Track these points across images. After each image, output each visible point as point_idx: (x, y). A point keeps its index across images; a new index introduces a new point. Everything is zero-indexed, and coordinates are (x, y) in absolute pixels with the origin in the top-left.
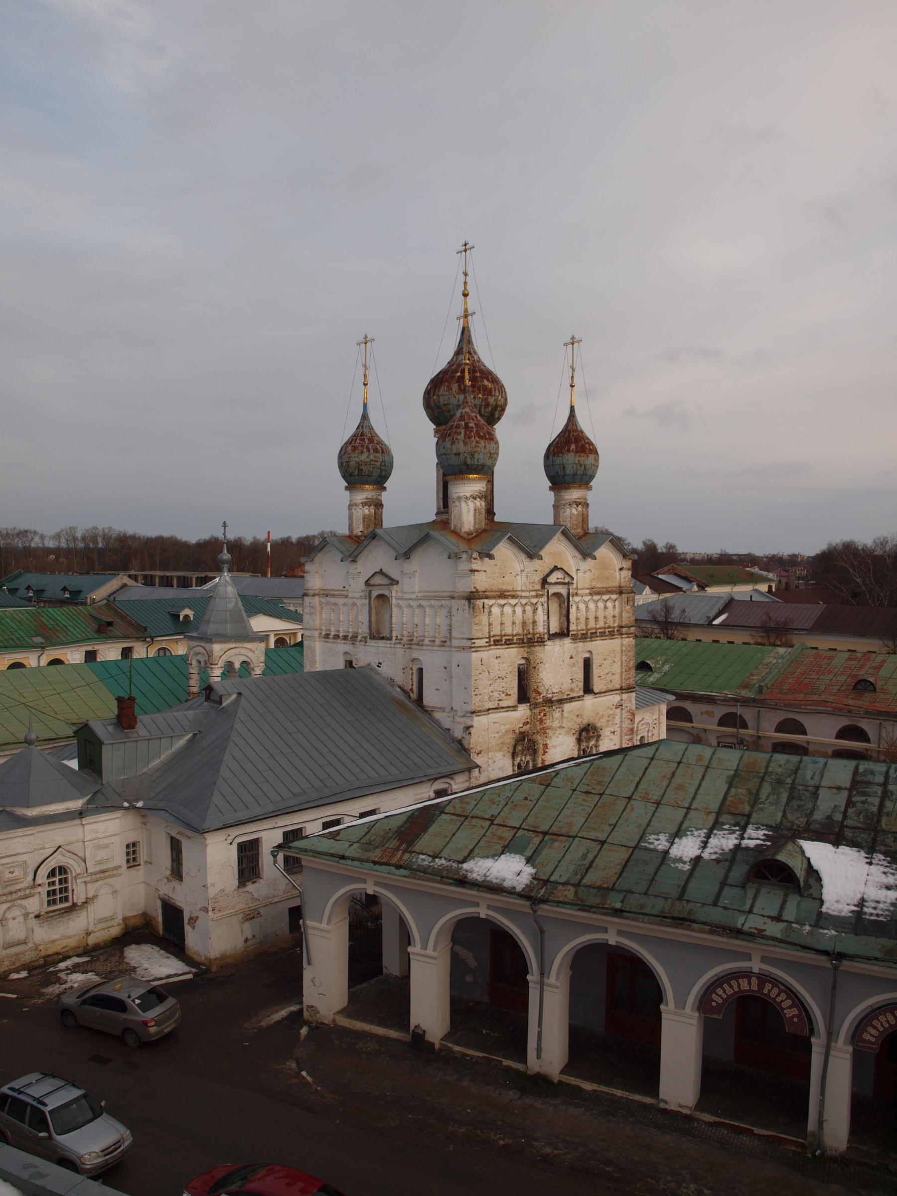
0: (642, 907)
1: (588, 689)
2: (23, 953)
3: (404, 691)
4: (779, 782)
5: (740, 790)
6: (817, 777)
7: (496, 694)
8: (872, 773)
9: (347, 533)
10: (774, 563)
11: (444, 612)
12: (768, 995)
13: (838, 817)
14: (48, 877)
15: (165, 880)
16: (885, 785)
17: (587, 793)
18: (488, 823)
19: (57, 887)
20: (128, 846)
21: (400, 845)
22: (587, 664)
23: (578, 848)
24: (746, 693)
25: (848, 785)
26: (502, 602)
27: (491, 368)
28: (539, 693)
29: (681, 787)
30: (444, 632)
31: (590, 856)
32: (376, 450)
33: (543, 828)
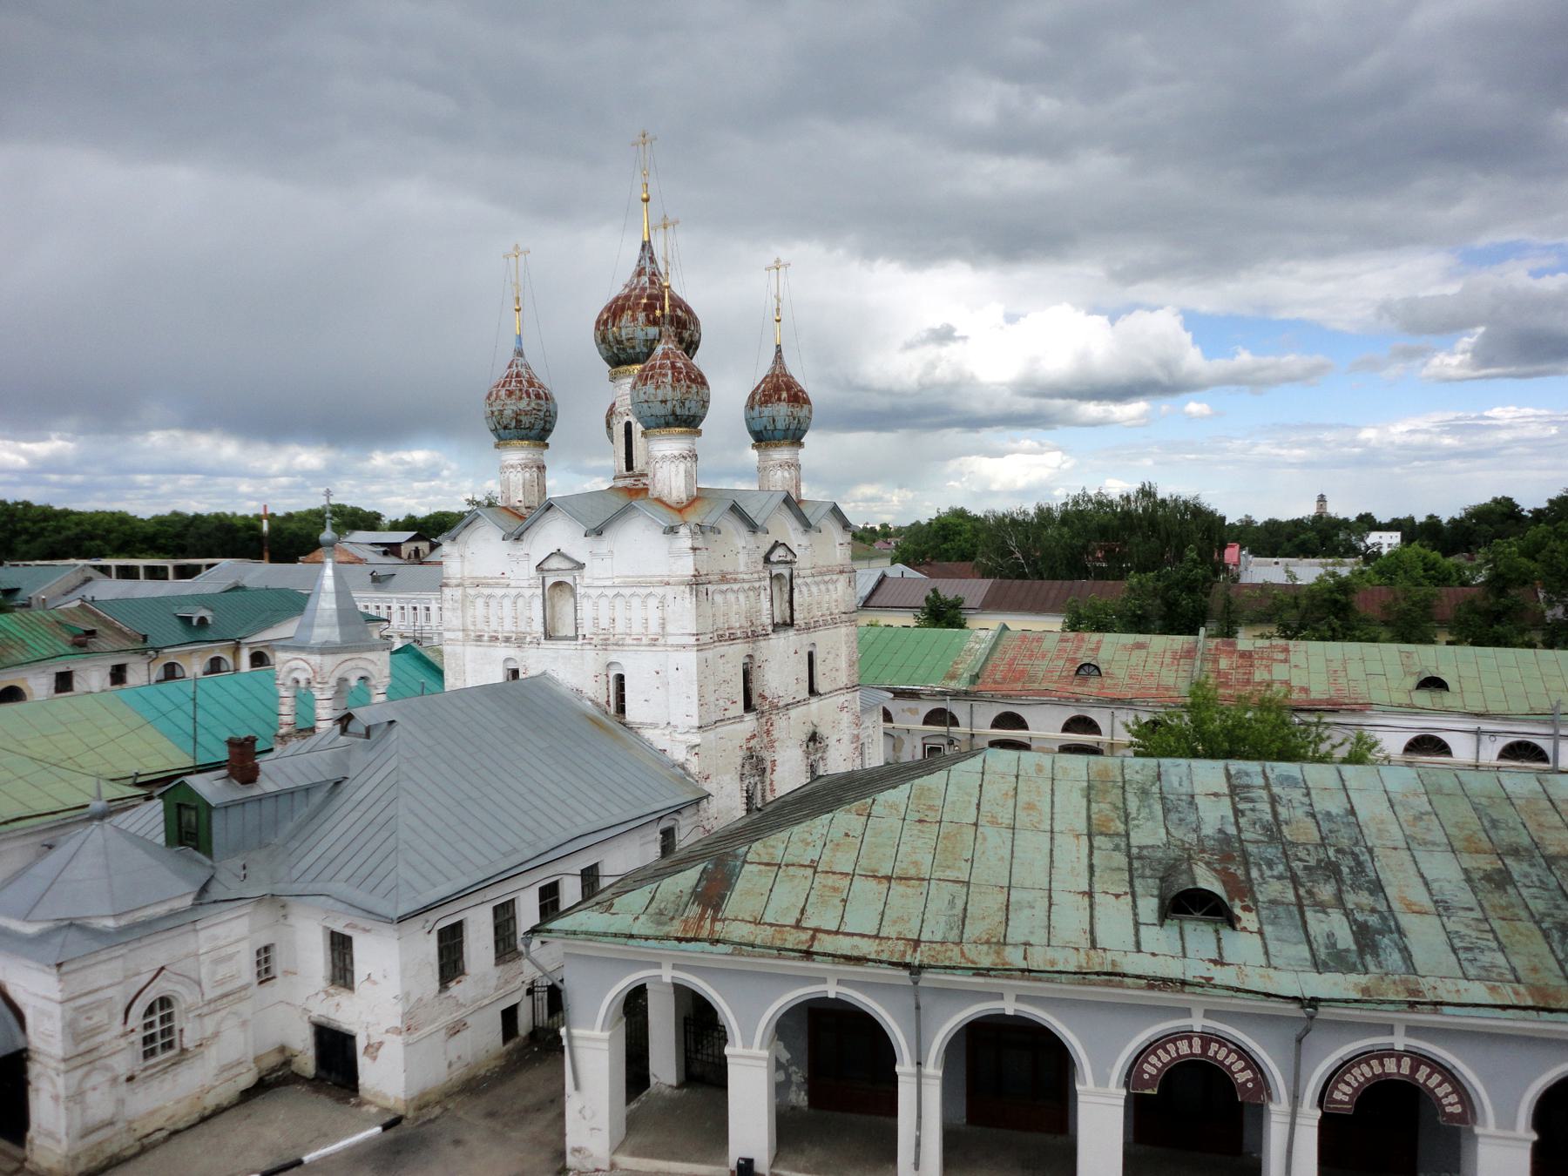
0: (1053, 963)
1: (812, 691)
2: (109, 1140)
3: (598, 705)
5: (1102, 805)
6: (1186, 783)
8: (1247, 774)
11: (653, 603)
12: (1214, 1058)
13: (1232, 830)
14: (145, 1016)
15: (322, 996)
17: (920, 821)
18: (810, 872)
19: (158, 1028)
20: (258, 953)
24: (954, 685)
28: (764, 698)
30: (654, 628)
31: (960, 904)
32: (538, 396)
33: (885, 870)
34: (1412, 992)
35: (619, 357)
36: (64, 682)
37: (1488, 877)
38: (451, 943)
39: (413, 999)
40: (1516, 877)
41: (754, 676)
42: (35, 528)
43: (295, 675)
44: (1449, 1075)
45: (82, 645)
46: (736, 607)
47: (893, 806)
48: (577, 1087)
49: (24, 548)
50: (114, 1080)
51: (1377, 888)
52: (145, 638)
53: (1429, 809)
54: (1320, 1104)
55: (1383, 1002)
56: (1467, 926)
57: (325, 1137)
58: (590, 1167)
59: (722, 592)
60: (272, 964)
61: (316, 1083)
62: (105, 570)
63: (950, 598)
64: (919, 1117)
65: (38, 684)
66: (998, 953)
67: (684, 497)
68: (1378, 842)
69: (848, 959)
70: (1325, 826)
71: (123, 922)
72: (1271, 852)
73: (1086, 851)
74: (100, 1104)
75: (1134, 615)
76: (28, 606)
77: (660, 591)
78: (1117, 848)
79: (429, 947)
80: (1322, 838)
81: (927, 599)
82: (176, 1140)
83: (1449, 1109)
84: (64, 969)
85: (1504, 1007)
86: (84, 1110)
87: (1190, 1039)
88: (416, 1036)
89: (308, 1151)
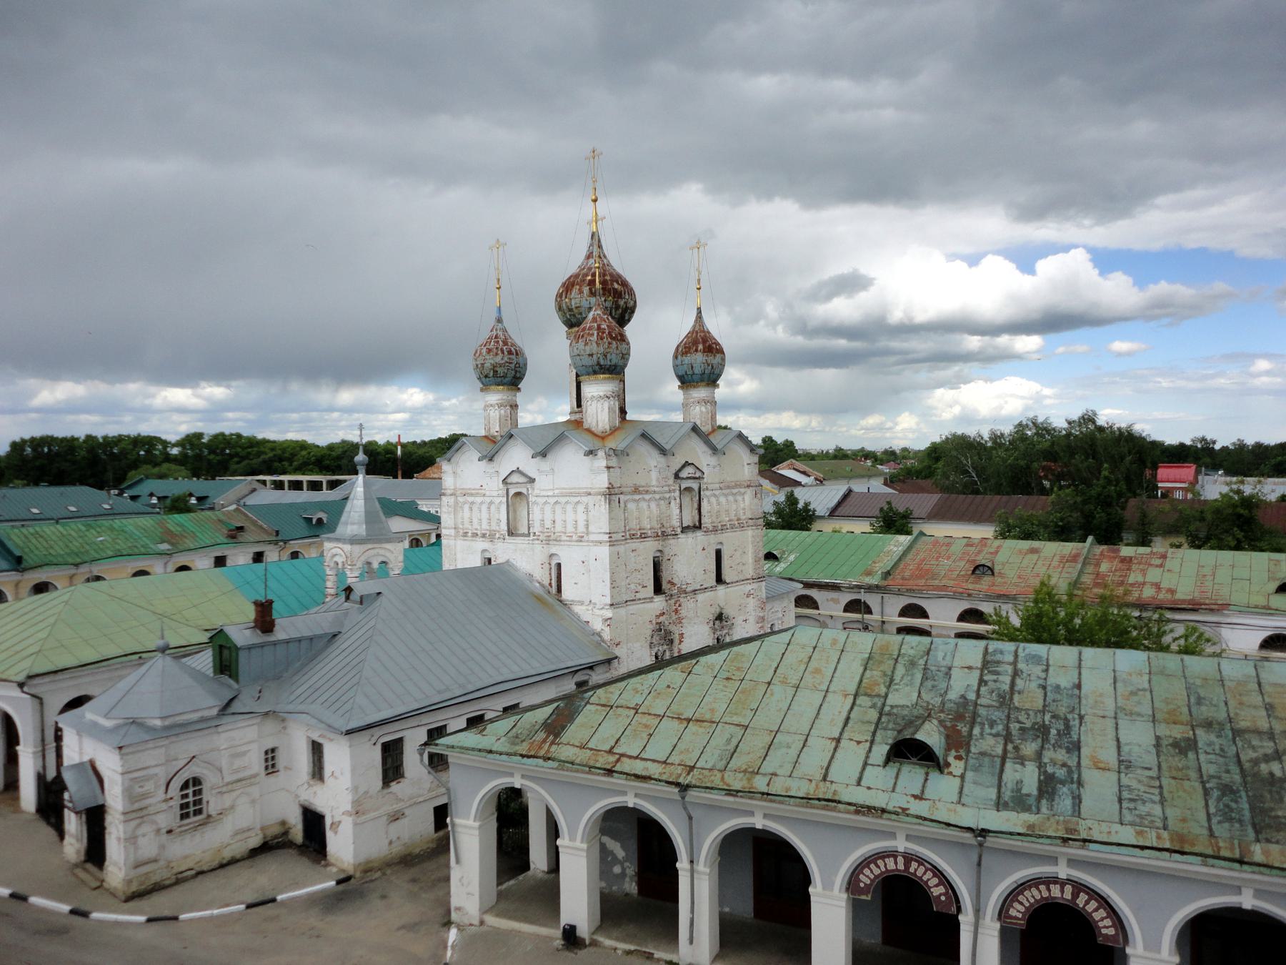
1: (719, 580)
2: (154, 872)
3: (543, 586)
4: (912, 664)
6: (948, 658)
7: (633, 586)
8: (1002, 652)
9: (483, 433)
10: (890, 456)
11: (581, 508)
13: (972, 696)
14: (182, 789)
16: (1015, 663)
17: (728, 679)
18: (633, 712)
19: (191, 799)
20: (266, 753)
21: (547, 737)
22: (718, 554)
23: (722, 734)
25: (979, 665)
26: (637, 497)
27: (621, 272)
28: (673, 584)
29: (817, 671)
30: (581, 528)
31: (734, 742)
32: (510, 352)
33: (688, 714)
34: (1068, 830)
35: (573, 320)
36: (220, 562)
37: (1175, 745)
38: (392, 757)
39: (361, 790)
40: (1200, 745)
41: (664, 567)
42: (243, 453)
43: (336, 559)
44: (1104, 902)
45: (233, 537)
46: (646, 513)
47: (711, 667)
48: (458, 861)
49: (235, 467)
50: (158, 831)
51: (1076, 747)
52: (277, 533)
53: (1147, 686)
54: (1000, 918)
55: (1041, 836)
56: (1140, 781)
57: (297, 885)
58: (467, 922)
59: (635, 500)
60: (276, 761)
61: (302, 849)
62: (264, 482)
63: (901, 510)
64: (693, 903)
65: (203, 562)
66: (749, 780)
67: (608, 427)
68: (1090, 711)
69: (637, 777)
70: (1050, 696)
71: (167, 723)
72: (997, 715)
73: (848, 707)
74: (148, 846)
75: (1057, 526)
76: (212, 509)
77: (585, 499)
78: (873, 706)
79: (375, 756)
80: (1044, 706)
81: (881, 509)
82: (200, 877)
83: (1104, 931)
84: (124, 751)
85: (1143, 848)
86: (136, 849)
87: (895, 857)
88: (363, 818)
89: (282, 892)
